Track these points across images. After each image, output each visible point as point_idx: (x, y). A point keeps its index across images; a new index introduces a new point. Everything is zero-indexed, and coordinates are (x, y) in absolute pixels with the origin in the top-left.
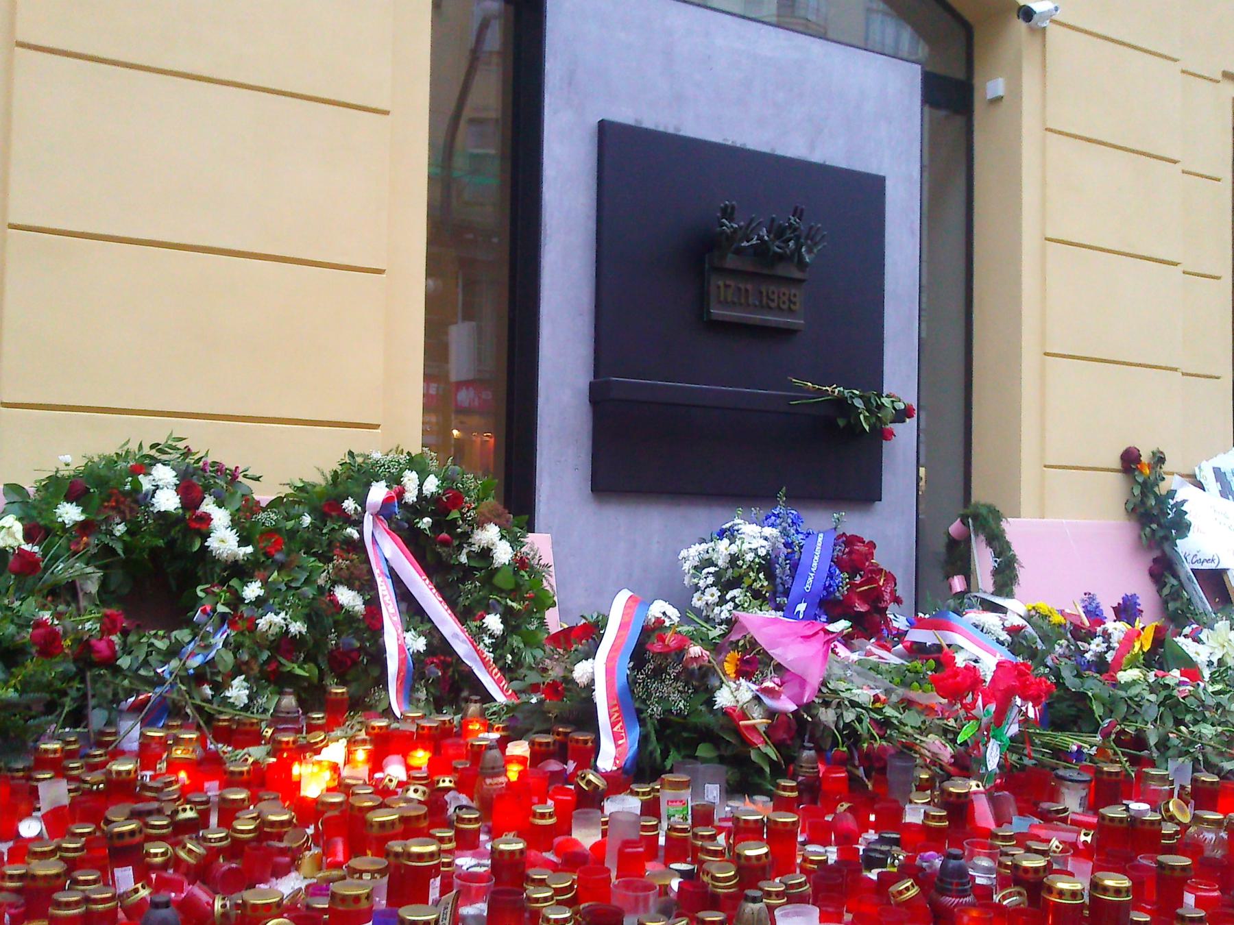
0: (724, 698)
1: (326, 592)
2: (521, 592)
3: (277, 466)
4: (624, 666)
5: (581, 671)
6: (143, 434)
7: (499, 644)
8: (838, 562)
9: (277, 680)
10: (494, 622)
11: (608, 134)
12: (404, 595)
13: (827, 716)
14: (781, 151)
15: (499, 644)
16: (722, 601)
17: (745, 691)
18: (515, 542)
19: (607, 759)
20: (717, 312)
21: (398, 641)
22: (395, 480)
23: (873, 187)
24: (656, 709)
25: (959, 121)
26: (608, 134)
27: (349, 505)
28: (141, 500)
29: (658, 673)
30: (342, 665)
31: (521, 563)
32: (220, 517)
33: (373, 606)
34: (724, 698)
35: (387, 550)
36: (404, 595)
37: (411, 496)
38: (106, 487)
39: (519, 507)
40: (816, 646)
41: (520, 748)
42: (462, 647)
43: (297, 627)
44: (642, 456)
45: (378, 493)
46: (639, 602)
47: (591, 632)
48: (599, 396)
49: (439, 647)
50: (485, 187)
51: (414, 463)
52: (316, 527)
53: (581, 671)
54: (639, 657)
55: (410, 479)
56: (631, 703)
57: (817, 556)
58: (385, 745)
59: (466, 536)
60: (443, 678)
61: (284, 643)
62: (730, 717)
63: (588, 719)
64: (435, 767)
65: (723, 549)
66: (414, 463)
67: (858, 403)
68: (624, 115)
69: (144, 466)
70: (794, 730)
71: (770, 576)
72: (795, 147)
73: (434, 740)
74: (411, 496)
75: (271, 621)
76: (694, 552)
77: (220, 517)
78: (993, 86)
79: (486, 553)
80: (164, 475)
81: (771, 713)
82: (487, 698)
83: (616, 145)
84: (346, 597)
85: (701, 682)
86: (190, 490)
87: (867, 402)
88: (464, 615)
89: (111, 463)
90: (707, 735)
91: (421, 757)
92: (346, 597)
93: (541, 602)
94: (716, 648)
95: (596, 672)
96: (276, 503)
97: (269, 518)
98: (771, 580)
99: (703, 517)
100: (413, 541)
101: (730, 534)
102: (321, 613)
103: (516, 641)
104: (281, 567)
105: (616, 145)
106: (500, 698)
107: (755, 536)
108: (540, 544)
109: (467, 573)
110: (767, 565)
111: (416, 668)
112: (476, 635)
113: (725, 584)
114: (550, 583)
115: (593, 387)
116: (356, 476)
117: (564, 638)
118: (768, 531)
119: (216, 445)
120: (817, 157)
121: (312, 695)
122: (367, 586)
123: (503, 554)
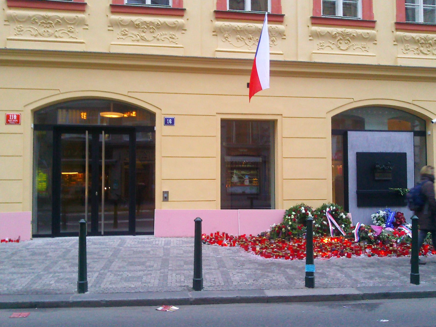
0: (369, 235)
1: (322, 222)
2: (347, 222)
3: (315, 206)
4: (358, 231)
5: (353, 231)
6: (299, 203)
7: (344, 228)
8: (395, 217)
9: (318, 233)
10: (343, 226)
11: (358, 154)
12: (331, 222)
13: (381, 237)
14: (387, 152)
15: (344, 228)
16: (377, 223)
17: (371, 234)
18: (346, 215)
19: (356, 241)
20: (376, 178)
21: (331, 228)
22: (329, 207)
23: (404, 156)
24: (361, 236)
25: (423, 138)
26: (358, 154)
27: (324, 211)
28: (300, 211)
29: (362, 232)
30: (325, 231)
31: (347, 218)
32: (310, 213)
33: (328, 224)
34: (369, 235)
35: (329, 216)
36: (331, 222)
37: (332, 209)
38: (296, 209)
39: (346, 210)
40: (380, 229)
41: (346, 239)
42: (339, 229)
43: (320, 226)
44: (365, 201)
45: (328, 209)
46: (360, 224)
47: (354, 227)
48: (358, 193)
49: (336, 229)
50: (341, 174)
51: (332, 205)
52: (320, 213)
53: (353, 231)
54: (359, 230)
55: (331, 207)
56: (358, 235)
57: (392, 215)
58: (332, 239)
59: (339, 215)
60: (337, 232)
61: (318, 228)
62: (369, 237)
63: (354, 237)
64: (337, 241)
65: (377, 215)
66: (332, 205)
67: (401, 191)
68: (360, 151)
69: (301, 207)
70: (378, 238)
71: (384, 219)
72: (390, 150)
73: (337, 238)
74: (332, 209)
75: (317, 225)
76: (373, 215)
77: (310, 213)
78: (429, 132)
79: (342, 216)
80: (303, 208)
81: (374, 236)
82: (343, 235)
83: (360, 156)
84: (325, 222)
85: (367, 233)
86: (306, 210)
87: (403, 191)
88: (339, 225)
89: (297, 207)
90: (367, 238)
91: (336, 240)
92: (325, 222)
93: (350, 223)
94: (369, 229)
95: (354, 231)
96: (315, 211)
97: (315, 213)
98: (384, 219)
99: (375, 209)
100: (332, 216)
101: (379, 213)
102: (322, 224)
103: (346, 228)
104: (317, 219)
105: (360, 156)
106: (344, 235)
107: (382, 213)
108: (349, 215)
109: (339, 219)
110: (384, 217)
111: (334, 231)
112: (341, 227)
113: (377, 220)
114: (351, 220)
115: (357, 191)
116: (324, 207)
117: (352, 228)
118: (384, 212)
119: (308, 204)
120: (393, 151)
121: (322, 234)
122: (327, 221)
123: (344, 217)
